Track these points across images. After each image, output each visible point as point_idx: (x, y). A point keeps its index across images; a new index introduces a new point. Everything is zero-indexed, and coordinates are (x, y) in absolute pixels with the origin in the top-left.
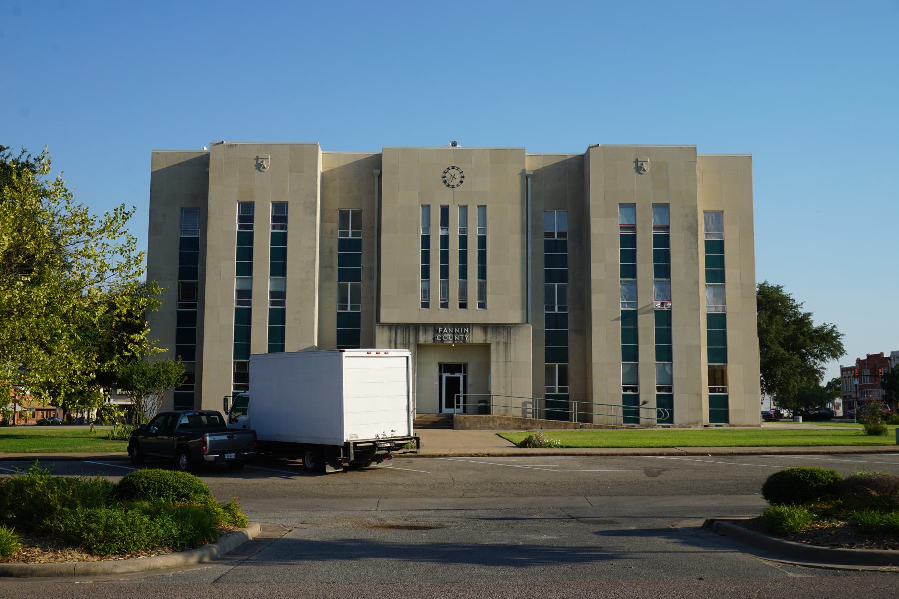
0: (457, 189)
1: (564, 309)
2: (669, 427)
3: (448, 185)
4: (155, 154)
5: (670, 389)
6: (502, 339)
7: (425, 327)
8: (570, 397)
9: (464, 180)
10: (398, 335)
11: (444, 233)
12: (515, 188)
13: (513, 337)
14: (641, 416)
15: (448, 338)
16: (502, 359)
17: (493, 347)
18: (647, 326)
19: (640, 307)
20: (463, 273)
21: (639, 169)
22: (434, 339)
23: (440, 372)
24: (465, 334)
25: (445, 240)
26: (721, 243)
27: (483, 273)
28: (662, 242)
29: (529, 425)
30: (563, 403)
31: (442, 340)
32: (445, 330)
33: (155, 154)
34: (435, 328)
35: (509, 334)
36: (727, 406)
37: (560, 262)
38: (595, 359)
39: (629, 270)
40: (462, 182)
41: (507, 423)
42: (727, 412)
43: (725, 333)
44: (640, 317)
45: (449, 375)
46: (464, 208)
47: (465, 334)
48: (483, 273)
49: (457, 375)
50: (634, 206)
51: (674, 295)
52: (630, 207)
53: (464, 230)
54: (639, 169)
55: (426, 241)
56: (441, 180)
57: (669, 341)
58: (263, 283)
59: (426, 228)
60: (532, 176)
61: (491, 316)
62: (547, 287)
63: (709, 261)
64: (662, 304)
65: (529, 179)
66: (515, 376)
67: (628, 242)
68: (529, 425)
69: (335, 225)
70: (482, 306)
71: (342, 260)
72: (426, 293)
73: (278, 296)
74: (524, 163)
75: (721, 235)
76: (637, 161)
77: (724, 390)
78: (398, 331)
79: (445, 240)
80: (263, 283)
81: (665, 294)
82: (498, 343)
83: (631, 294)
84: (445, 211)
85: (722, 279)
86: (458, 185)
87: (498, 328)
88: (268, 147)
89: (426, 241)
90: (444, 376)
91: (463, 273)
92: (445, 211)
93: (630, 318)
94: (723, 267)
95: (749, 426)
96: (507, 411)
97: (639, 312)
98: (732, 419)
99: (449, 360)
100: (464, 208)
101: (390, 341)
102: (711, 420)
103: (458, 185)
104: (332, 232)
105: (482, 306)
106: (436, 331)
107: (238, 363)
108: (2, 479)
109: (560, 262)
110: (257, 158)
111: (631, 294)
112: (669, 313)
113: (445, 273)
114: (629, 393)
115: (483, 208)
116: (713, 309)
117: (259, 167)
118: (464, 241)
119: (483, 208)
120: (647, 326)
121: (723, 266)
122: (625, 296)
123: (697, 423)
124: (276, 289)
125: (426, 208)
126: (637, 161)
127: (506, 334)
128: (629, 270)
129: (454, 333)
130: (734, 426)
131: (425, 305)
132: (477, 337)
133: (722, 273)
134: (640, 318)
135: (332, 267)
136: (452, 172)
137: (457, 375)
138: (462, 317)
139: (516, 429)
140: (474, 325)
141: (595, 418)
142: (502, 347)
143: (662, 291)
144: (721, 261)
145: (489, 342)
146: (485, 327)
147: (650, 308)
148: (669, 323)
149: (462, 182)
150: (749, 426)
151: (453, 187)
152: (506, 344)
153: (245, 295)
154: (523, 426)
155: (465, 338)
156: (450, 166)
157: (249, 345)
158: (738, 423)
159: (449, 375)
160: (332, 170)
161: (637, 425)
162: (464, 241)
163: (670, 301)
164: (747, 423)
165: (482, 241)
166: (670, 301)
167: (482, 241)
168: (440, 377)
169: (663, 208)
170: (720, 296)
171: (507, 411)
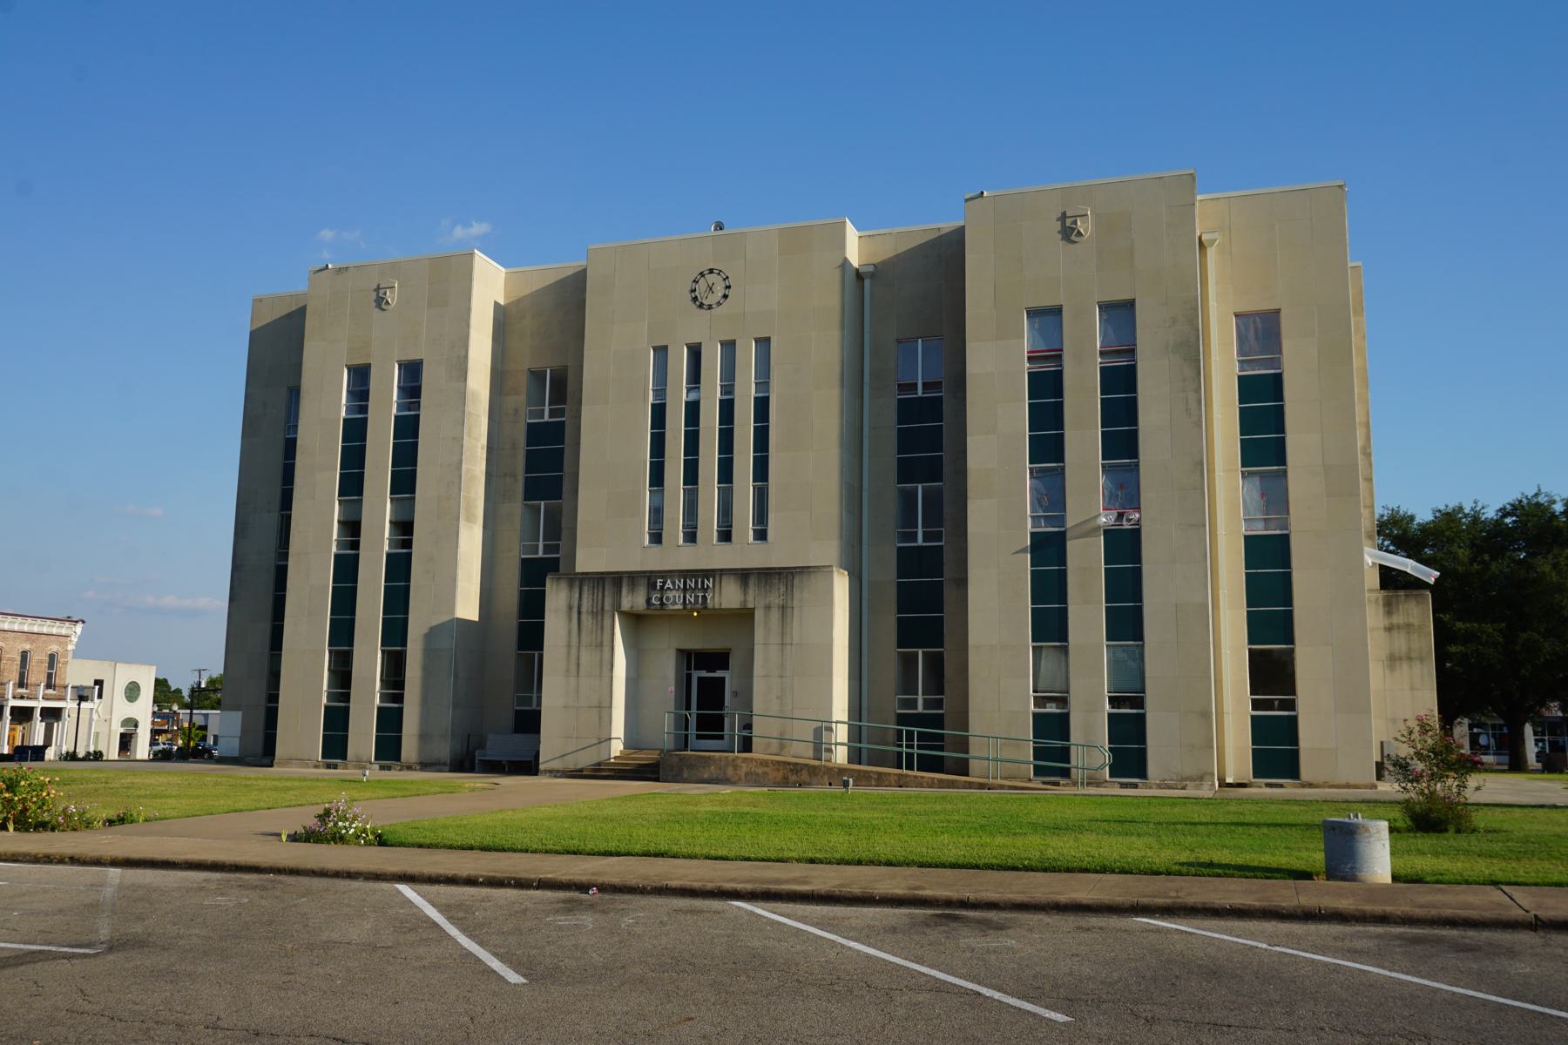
0: (717, 311)
1: (938, 536)
2: (1135, 786)
3: (701, 306)
4: (257, 301)
5: (1139, 702)
6: (775, 599)
7: (633, 577)
8: (947, 721)
9: (731, 293)
10: (585, 595)
11: (693, 396)
12: (829, 298)
13: (797, 595)
14: (1073, 762)
15: (675, 600)
16: (775, 638)
17: (759, 615)
18: (1087, 566)
19: (1070, 523)
20: (726, 473)
21: (1068, 233)
22: (648, 601)
23: (689, 668)
24: (705, 590)
25: (693, 410)
26: (1277, 380)
27: (761, 470)
28: (1120, 384)
29: (805, 776)
30: (919, 726)
31: (662, 604)
32: (669, 584)
33: (257, 301)
34: (650, 579)
35: (790, 588)
36: (1294, 740)
37: (917, 439)
38: (973, 639)
39: (1047, 445)
40: (725, 296)
41: (760, 771)
42: (1295, 755)
43: (1287, 578)
44: (1069, 544)
45: (704, 674)
46: (729, 347)
47: (705, 590)
48: (761, 470)
49: (719, 674)
50: (1057, 311)
51: (1147, 495)
52: (1048, 316)
53: (728, 389)
54: (1068, 233)
55: (659, 413)
56: (689, 297)
57: (1137, 595)
58: (380, 510)
59: (660, 392)
60: (872, 275)
61: (773, 555)
62: (902, 492)
63: (1249, 421)
64: (1120, 516)
65: (867, 282)
66: (819, 671)
67: (1047, 389)
68: (805, 776)
69: (518, 400)
70: (761, 535)
71: (532, 461)
72: (657, 513)
73: (404, 527)
74: (842, 245)
75: (1276, 363)
76: (1064, 216)
77: (1291, 705)
78: (585, 588)
79: (693, 410)
80: (380, 510)
81: (1126, 490)
82: (768, 608)
83: (1052, 493)
84: (695, 353)
85: (1281, 458)
86: (719, 304)
87: (768, 576)
88: (394, 268)
89: (659, 413)
90: (696, 675)
91: (726, 473)
92: (695, 353)
93: (1049, 550)
94: (1282, 430)
95: (1348, 786)
96: (782, 747)
97: (1068, 535)
98: (1306, 772)
99: (695, 643)
100: (729, 347)
101: (570, 608)
102: (1259, 771)
103: (719, 304)
104: (516, 410)
105: (761, 535)
106: (652, 586)
107: (337, 652)
108: (1551, 764)
109: (917, 439)
110: (378, 289)
111: (1052, 493)
112: (1135, 535)
113: (691, 475)
114: (1052, 709)
115: (764, 343)
116: (1261, 525)
117: (380, 302)
118: (727, 409)
119: (764, 343)
120: (1087, 566)
121: (1281, 428)
122: (1037, 502)
123: (1201, 778)
124: (400, 518)
125: (662, 351)
126: (1064, 214)
127: (783, 589)
128: (1047, 445)
129: (685, 589)
130: (1311, 785)
131: (657, 538)
132: (728, 596)
133: (1280, 446)
134: (1072, 546)
135: (514, 476)
136: (711, 278)
137: (719, 674)
138: (710, 554)
139: (778, 785)
140: (722, 572)
141: (974, 765)
142: (775, 615)
143: (1121, 487)
144: (1276, 420)
145: (750, 605)
146: (744, 576)
147: (1091, 525)
148: (1136, 557)
149: (725, 296)
150: (1348, 786)
151: (710, 307)
152: (783, 608)
153: (352, 527)
154: (793, 778)
155: (704, 598)
156: (705, 268)
157: (353, 621)
158: (1321, 779)
159: (704, 674)
160: (519, 301)
161: (1063, 781)
162: (727, 409)
163: (1138, 508)
164: (1344, 782)
165: (762, 406)
166: (1138, 508)
167: (762, 406)
168: (689, 677)
169: (1120, 313)
170: (1275, 497)
171: (782, 747)
